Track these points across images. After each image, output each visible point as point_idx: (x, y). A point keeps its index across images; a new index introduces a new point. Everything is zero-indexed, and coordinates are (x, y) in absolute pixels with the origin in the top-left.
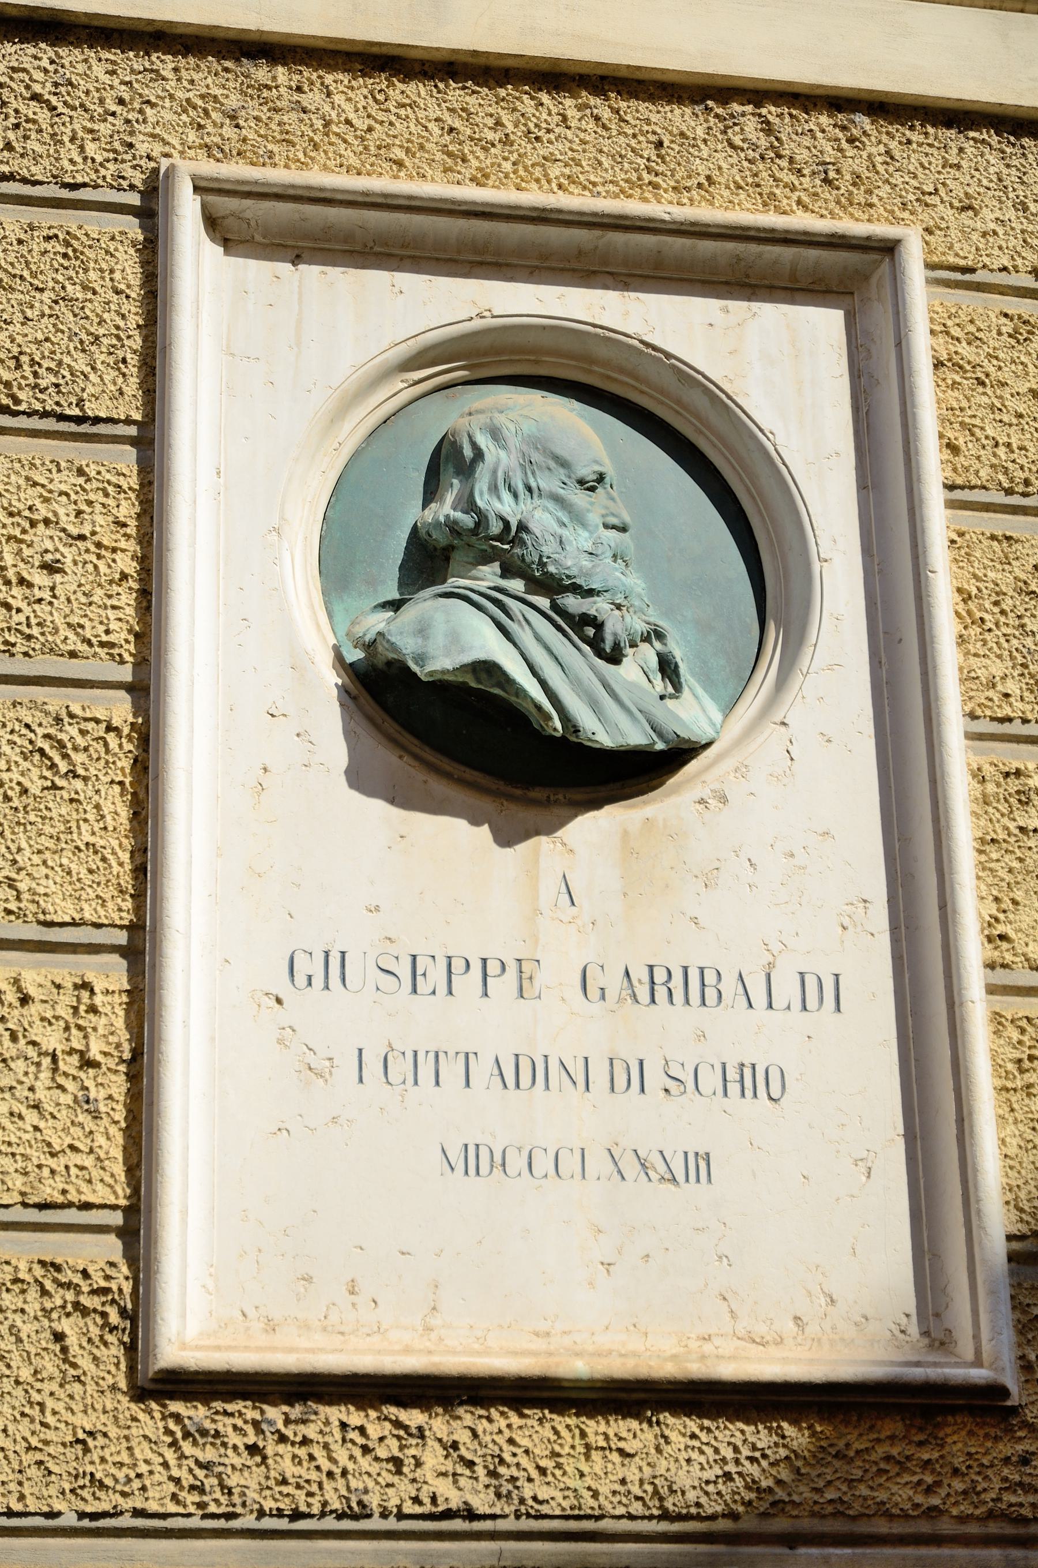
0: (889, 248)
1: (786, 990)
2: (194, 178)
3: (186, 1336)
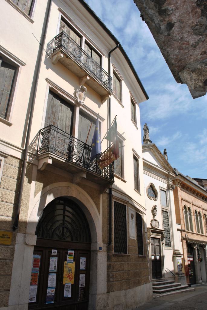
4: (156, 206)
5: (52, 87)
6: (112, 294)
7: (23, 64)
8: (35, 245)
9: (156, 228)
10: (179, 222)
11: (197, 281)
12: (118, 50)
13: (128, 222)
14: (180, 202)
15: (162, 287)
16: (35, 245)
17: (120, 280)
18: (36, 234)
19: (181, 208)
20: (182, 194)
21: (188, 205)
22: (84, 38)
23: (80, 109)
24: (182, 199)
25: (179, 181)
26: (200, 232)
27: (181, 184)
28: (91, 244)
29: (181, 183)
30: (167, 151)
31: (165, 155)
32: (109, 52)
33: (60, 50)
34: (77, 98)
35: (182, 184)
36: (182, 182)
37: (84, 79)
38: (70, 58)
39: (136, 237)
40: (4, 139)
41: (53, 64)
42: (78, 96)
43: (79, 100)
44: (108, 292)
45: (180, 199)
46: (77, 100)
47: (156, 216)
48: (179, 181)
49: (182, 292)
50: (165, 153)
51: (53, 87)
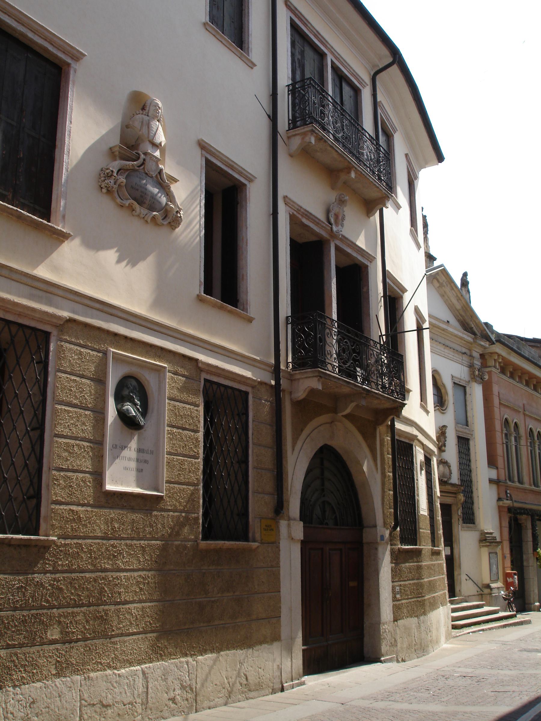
0: (247, 393)
1: (149, 452)
2: (205, 379)
3: (109, 487)
4: (445, 426)
5: (293, 213)
6: (400, 622)
7: (77, 56)
8: (302, 538)
9: (446, 479)
10: (492, 462)
11: (526, 606)
12: (395, 69)
13: (417, 480)
14: (496, 410)
15: (468, 615)
16: (302, 538)
17: (410, 597)
18: (301, 520)
19: (498, 425)
20: (503, 386)
21: (514, 418)
22: (329, 58)
23: (336, 244)
24: (500, 404)
25: (496, 358)
26: (516, 479)
27: (499, 363)
28: (364, 531)
29: (500, 360)
30: (469, 278)
31: (463, 289)
32: (372, 74)
33: (311, 128)
34: (331, 224)
35: (502, 365)
36: (503, 358)
37: (343, 177)
38: (325, 141)
39: (426, 511)
40: (85, 291)
41: (291, 156)
42: (332, 221)
43: (335, 229)
44: (395, 620)
45: (496, 402)
46: (331, 228)
47: (444, 451)
48: (496, 358)
49: (505, 626)
50: (465, 283)
51: (295, 213)
